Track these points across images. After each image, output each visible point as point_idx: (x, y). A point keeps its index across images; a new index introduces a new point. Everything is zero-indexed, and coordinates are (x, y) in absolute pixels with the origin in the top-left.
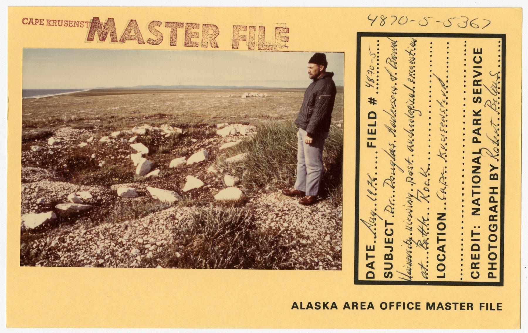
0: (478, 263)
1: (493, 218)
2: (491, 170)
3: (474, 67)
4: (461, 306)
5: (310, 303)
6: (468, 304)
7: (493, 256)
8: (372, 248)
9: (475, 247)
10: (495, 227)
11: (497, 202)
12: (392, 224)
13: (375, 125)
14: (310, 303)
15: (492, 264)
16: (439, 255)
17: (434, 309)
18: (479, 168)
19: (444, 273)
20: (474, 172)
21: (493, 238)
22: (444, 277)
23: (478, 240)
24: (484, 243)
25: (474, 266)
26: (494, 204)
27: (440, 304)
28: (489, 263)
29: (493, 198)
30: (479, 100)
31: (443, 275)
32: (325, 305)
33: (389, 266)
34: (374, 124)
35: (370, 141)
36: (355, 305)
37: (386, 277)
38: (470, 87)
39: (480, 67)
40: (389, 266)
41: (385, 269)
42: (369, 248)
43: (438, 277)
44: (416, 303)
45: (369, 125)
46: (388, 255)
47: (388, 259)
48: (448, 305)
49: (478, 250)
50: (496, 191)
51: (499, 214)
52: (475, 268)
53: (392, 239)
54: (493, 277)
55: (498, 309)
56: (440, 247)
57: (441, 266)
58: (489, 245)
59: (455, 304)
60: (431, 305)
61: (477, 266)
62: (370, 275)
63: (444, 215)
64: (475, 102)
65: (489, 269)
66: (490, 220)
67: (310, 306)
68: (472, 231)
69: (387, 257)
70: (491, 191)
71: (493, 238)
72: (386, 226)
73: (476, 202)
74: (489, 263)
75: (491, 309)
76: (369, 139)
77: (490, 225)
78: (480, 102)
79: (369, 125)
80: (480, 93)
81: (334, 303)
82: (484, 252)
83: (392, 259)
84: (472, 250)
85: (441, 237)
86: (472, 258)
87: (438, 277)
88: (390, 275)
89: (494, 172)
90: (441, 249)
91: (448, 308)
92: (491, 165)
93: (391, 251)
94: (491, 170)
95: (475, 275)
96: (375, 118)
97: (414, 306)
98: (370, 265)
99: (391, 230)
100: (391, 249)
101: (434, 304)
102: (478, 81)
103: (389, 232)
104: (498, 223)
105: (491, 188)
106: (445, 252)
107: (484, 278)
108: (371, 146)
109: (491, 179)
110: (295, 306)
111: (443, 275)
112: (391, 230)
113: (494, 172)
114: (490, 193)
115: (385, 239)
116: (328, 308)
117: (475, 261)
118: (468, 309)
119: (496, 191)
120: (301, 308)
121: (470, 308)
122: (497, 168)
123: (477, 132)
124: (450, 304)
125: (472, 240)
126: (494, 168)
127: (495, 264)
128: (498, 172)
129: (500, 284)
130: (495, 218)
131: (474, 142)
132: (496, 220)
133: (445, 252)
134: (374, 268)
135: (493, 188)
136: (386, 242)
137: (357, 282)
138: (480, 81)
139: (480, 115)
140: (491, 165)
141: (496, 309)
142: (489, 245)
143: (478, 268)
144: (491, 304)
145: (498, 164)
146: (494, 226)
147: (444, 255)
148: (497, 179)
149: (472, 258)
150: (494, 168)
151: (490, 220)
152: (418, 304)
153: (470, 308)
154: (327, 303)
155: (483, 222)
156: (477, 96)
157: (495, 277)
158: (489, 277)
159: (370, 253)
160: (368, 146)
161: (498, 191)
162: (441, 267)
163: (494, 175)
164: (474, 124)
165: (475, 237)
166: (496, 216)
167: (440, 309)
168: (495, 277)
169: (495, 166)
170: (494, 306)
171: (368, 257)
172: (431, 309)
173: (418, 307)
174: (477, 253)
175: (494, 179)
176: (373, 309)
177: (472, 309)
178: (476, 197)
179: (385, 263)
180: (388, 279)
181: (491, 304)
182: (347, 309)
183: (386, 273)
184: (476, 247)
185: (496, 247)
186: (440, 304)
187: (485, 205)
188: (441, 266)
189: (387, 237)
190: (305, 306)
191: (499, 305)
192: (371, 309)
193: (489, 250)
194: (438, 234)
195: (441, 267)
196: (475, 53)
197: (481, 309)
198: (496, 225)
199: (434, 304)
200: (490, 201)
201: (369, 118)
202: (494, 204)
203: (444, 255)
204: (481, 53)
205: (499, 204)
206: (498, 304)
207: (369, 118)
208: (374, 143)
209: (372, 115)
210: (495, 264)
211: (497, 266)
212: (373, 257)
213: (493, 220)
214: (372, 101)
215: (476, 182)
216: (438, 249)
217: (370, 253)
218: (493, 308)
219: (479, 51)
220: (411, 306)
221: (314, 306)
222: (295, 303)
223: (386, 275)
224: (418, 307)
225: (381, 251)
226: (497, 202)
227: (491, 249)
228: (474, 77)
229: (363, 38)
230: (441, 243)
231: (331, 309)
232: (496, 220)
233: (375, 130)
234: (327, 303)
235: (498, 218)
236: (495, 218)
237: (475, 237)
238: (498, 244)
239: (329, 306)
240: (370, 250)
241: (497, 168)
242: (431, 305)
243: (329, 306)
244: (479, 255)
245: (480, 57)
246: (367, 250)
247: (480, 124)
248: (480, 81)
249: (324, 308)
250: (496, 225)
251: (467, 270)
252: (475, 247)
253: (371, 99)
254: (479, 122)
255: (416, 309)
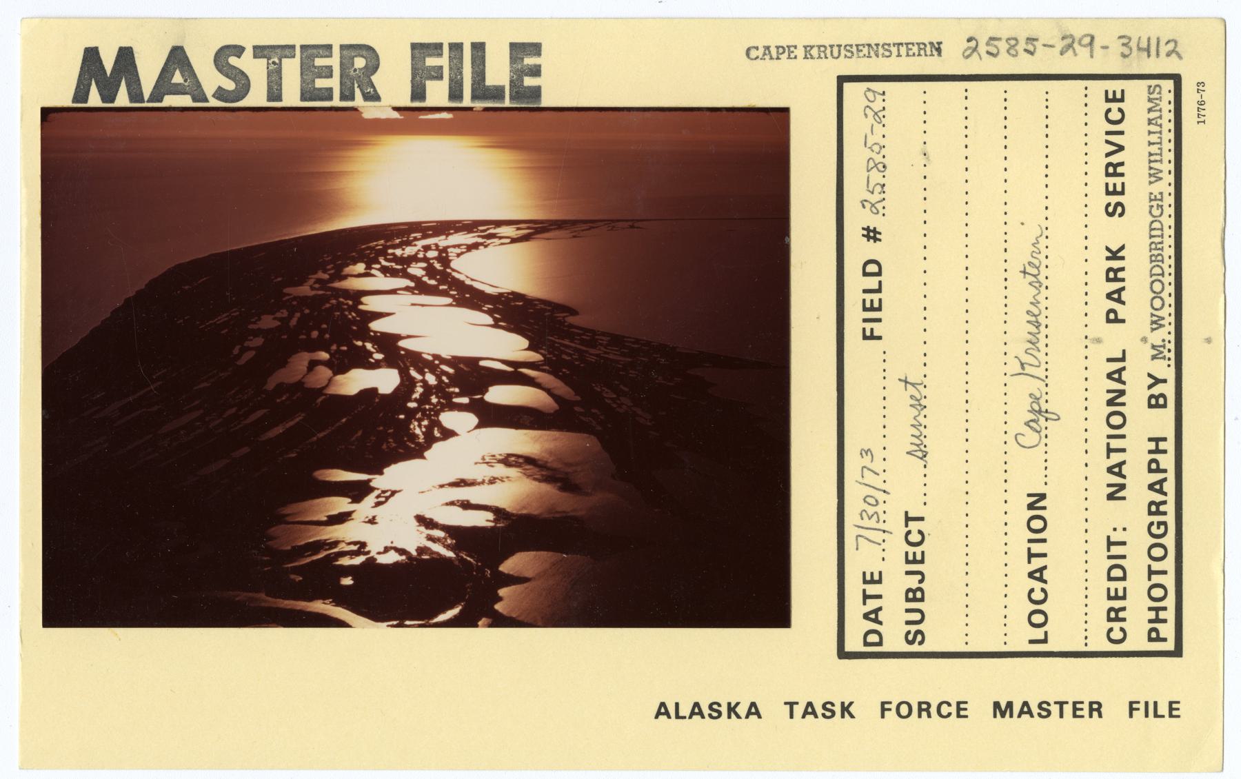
0: (1124, 609)
1: (1158, 508)
2: (1150, 387)
3: (1108, 133)
4: (1075, 709)
5: (696, 705)
6: (1091, 703)
7: (1158, 593)
8: (876, 577)
9: (1117, 573)
10: (1162, 527)
11: (1165, 471)
12: (922, 519)
13: (879, 290)
14: (696, 705)
15: (1157, 610)
16: (1032, 591)
17: (1011, 716)
18: (1122, 393)
19: (1046, 633)
20: (1110, 403)
21: (1158, 552)
22: (1045, 641)
23: (1124, 557)
24: (1137, 563)
25: (1115, 615)
26: (1160, 476)
27: (1025, 704)
28: (1150, 609)
29: (1156, 630)
30: (1119, 210)
31: (1042, 637)
32: (732, 709)
33: (917, 616)
34: (877, 287)
35: (868, 326)
36: (924, 708)
37: (911, 643)
38: (1099, 180)
39: (1122, 133)
40: (917, 616)
41: (908, 623)
42: (868, 578)
43: (1031, 642)
44: (959, 703)
45: (865, 291)
46: (914, 592)
47: (915, 600)
48: (1044, 706)
49: (1124, 578)
50: (1162, 445)
51: (1171, 498)
52: (1117, 619)
53: (923, 553)
54: (1159, 639)
55: (1171, 716)
56: (1036, 571)
57: (1038, 615)
58: (1149, 566)
59: (1061, 704)
60: (1003, 708)
61: (1121, 615)
62: (873, 638)
63: (1042, 497)
64: (1111, 215)
65: (1150, 452)
66: (1150, 513)
67: (696, 710)
68: (1108, 537)
69: (911, 595)
70: (1152, 446)
71: (1158, 552)
72: (907, 526)
73: (1116, 470)
74: (1150, 609)
75: (1156, 715)
76: (865, 320)
77: (1152, 524)
78: (1121, 215)
79: (865, 291)
80: (1122, 193)
81: (753, 704)
82: (1137, 584)
83: (922, 600)
84: (1110, 579)
85: (1036, 548)
86: (1110, 598)
87: (1031, 642)
88: (919, 638)
89: (1156, 390)
90: (1037, 575)
91: (1044, 713)
92: (1150, 375)
93: (921, 581)
94: (1150, 387)
95: (1116, 635)
96: (879, 274)
97: (953, 709)
98: (873, 616)
99: (920, 532)
100: (919, 577)
101: (1010, 705)
102: (1115, 166)
103: (915, 538)
104: (1170, 519)
105: (1150, 440)
106: (1045, 582)
107: (1139, 641)
108: (870, 337)
109: (1150, 406)
110: (1026, 709)
111: (1042, 637)
112: (920, 532)
113: (1156, 390)
114: (1150, 452)
115: (907, 553)
116: (738, 717)
117: (1117, 604)
118: (1091, 716)
119: (1162, 445)
120: (678, 717)
121: (1095, 714)
122: (1165, 381)
123: (1116, 296)
124: (1049, 704)
125: (1110, 557)
126: (1157, 381)
127: (1165, 609)
128: (1169, 389)
129: (1178, 652)
130: (1162, 508)
131: (1109, 321)
132: (1165, 513)
133: (1045, 582)
134: (880, 623)
135: (1157, 440)
136: (908, 562)
137: (843, 654)
138: (1122, 164)
139: (1123, 258)
140: (1150, 375)
141: (1167, 714)
142: (1149, 566)
143: (1124, 620)
144: (1156, 703)
145: (1170, 374)
146: (1159, 524)
147: (1043, 590)
148: (1165, 406)
149: (1110, 598)
150: (1157, 381)
151: (1150, 513)
152: (962, 706)
153: (1095, 714)
154: (738, 704)
155: (1132, 515)
156: (1114, 199)
157: (1165, 640)
158: (1150, 639)
159: (872, 589)
160: (865, 338)
161: (1169, 445)
162: (1038, 619)
163: (1157, 398)
164: (1108, 280)
165: (1115, 550)
166: (1164, 503)
167: (1026, 717)
168: (1165, 640)
169: (1160, 377)
170: (1163, 709)
171: (866, 597)
172: (1003, 715)
173: (962, 713)
174: (1120, 585)
175: (1157, 406)
176: (760, 717)
177: (1100, 716)
178: (1116, 458)
179: (908, 611)
180: (915, 648)
181: (1156, 703)
182: (663, 718)
183: (909, 632)
184: (1117, 571)
185: (1165, 572)
186: (1025, 704)
187: (1138, 479)
188: (1038, 615)
189: (911, 550)
190: (685, 710)
191: (1174, 706)
192: (753, 718)
193: (1150, 579)
194: (1030, 541)
195: (1038, 619)
196: (1108, 100)
197: (1131, 716)
198: (1165, 523)
199: (1010, 705)
200: (1150, 471)
201: (865, 274)
202: (1160, 476)
203: (1043, 590)
204: (1122, 100)
205: (1171, 475)
206: (1171, 703)
207: (865, 274)
208: (878, 329)
209: (872, 268)
210: (1165, 609)
211: (1170, 615)
212: (880, 597)
213: (1158, 513)
214: (872, 234)
215: (1116, 424)
216: (1031, 575)
217: (872, 589)
218: (1159, 713)
219: (1119, 96)
220: (945, 710)
221: (706, 711)
222: (663, 704)
223: (910, 637)
224: (962, 713)
225: (896, 584)
226: (1165, 471)
227: (1153, 577)
228: (1108, 155)
229: (847, 86)
230: (1037, 563)
231: (747, 717)
232: (1165, 513)
233: (880, 300)
234: (738, 704)
235: (1170, 508)
236: (1162, 508)
237: (1115, 550)
238: (1169, 564)
239: (742, 710)
240: (872, 581)
241: (1165, 381)
242: (1003, 708)
243: (742, 710)
244: (1125, 589)
245: (1120, 110)
246: (865, 582)
247: (1123, 280)
248: (1122, 164)
249: (843, 716)
250: (1165, 523)
251: (1100, 624)
252: (1117, 573)
253: (876, 240)
254: (1120, 275)
255: (959, 716)
